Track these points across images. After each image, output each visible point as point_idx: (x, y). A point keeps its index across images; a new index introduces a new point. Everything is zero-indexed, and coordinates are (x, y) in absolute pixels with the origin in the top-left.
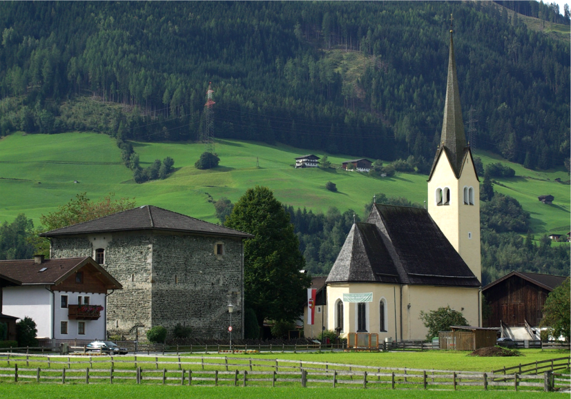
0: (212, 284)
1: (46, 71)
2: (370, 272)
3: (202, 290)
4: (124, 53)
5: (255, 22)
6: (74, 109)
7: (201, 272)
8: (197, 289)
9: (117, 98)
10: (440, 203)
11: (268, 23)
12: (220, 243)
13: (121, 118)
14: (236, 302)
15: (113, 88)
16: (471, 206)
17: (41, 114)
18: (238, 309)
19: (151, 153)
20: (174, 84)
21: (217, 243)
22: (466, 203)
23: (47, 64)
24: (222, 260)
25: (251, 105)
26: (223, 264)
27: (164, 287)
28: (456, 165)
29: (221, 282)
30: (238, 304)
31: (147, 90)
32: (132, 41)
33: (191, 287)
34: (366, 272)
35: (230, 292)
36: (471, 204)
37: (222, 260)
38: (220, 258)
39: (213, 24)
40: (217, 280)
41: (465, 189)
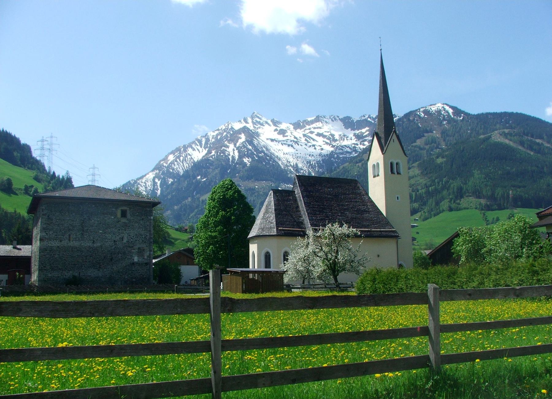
0: (115, 241)
1: (455, 190)
2: (274, 228)
3: (101, 246)
4: (483, 182)
5: (529, 167)
6: (464, 202)
7: (100, 231)
8: (95, 245)
9: (479, 197)
10: (374, 177)
11: (534, 168)
12: (124, 208)
13: (480, 204)
14: (143, 256)
15: (478, 194)
16: (399, 175)
17: (453, 206)
18: (146, 261)
19: (491, 215)
20: (499, 191)
21: (120, 208)
22: (392, 172)
23: (456, 188)
24: (127, 222)
25: (527, 196)
26: (128, 225)
27: (55, 244)
28: (383, 141)
29: (125, 241)
30: (146, 257)
31: (489, 193)
32: (485, 178)
33: (90, 244)
34: (271, 227)
35: (136, 247)
36: (400, 174)
37: (127, 222)
38: (124, 220)
39: (514, 169)
40: (120, 238)
41: (392, 164)
